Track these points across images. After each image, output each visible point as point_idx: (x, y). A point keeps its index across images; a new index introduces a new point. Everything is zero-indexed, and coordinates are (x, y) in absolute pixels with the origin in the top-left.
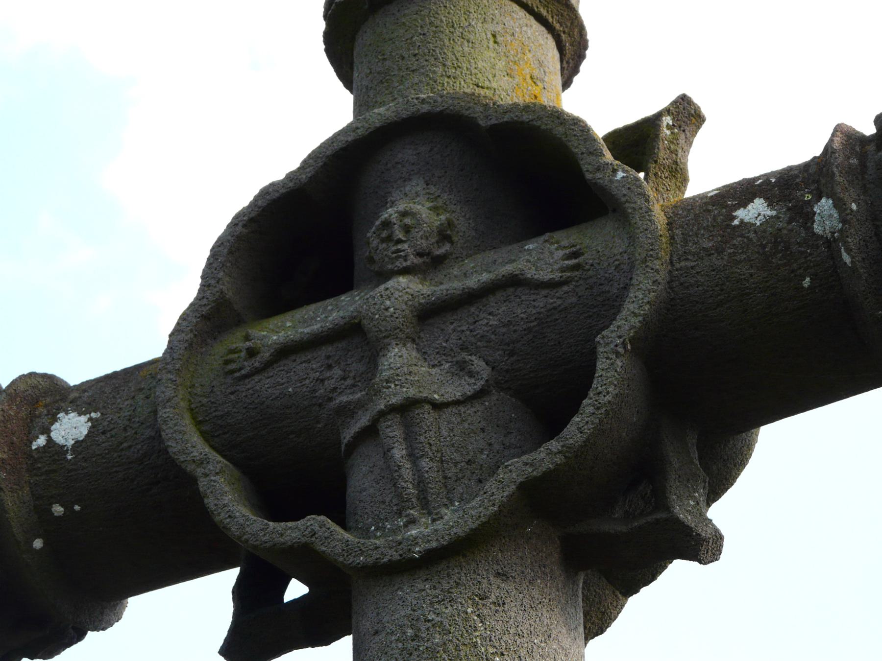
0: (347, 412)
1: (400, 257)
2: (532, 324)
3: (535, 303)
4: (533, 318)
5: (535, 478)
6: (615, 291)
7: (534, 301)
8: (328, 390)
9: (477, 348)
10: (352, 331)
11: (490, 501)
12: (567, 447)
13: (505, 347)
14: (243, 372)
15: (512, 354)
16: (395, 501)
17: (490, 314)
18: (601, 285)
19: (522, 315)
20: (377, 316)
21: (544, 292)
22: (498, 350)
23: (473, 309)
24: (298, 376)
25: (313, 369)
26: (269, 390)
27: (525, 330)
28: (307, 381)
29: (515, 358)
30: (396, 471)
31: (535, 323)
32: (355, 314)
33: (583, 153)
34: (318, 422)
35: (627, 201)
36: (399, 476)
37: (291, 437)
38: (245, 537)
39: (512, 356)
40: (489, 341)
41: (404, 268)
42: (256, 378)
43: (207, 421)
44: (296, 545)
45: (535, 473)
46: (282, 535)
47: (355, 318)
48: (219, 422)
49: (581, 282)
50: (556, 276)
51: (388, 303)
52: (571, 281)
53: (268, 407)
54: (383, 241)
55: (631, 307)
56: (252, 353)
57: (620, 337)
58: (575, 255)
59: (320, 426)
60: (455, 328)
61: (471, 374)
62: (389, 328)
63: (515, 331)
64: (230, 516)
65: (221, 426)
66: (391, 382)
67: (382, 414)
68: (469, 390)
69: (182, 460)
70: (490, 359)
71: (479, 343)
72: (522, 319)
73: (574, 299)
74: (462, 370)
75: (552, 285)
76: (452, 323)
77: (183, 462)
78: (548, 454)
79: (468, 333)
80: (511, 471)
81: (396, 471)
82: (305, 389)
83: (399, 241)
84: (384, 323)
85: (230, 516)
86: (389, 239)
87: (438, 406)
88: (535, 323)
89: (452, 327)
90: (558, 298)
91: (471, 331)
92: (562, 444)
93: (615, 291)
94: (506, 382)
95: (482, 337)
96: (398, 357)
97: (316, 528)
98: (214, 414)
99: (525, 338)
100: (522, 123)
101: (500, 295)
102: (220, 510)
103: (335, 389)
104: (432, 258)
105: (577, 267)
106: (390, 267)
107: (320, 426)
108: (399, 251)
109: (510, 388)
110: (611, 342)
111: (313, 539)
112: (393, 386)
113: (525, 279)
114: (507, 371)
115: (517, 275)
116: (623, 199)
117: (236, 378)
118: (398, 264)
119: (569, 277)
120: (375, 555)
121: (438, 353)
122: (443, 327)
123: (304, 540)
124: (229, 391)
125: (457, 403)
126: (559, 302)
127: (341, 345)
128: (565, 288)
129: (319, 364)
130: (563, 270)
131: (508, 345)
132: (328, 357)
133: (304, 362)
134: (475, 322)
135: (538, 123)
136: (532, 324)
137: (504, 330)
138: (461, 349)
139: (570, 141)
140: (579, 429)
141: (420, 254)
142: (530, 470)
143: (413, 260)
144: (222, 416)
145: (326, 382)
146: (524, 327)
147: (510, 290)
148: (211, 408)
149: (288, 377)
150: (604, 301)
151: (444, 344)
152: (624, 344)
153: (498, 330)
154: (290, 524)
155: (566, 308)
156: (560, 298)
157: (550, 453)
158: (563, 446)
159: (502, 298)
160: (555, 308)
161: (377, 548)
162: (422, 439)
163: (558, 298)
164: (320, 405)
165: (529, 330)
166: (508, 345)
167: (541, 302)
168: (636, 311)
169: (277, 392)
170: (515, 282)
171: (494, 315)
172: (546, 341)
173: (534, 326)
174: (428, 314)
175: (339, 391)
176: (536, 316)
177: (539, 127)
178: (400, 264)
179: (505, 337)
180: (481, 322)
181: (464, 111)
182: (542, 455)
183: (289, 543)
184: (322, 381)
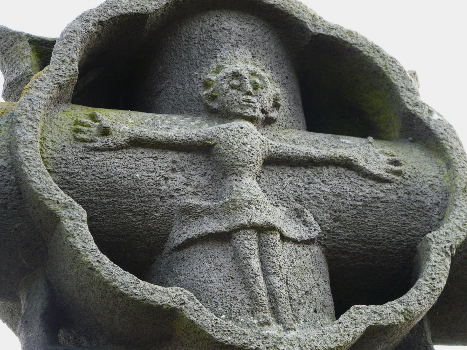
0: (190, 213)
1: (250, 106)
2: (358, 203)
3: (362, 188)
4: (359, 199)
5: (382, 326)
6: (429, 204)
7: (361, 185)
8: (171, 188)
9: (309, 204)
10: (203, 150)
11: (345, 331)
12: (408, 311)
13: (333, 213)
14: (96, 145)
15: (335, 220)
16: (247, 301)
17: (323, 181)
18: (417, 194)
19: (351, 193)
20: (236, 147)
21: (371, 182)
22: (326, 212)
23: (309, 172)
24: (145, 169)
25: (160, 167)
26: (118, 169)
27: (351, 205)
28: (153, 174)
29: (337, 224)
30: (253, 278)
31: (361, 203)
32: (210, 137)
33: (402, 87)
34: (156, 211)
35: (444, 139)
36: (255, 282)
37: (127, 214)
38: (114, 283)
39: (335, 221)
40: (320, 203)
41: (253, 116)
42: (107, 154)
43: (55, 172)
44: (165, 307)
45: (382, 322)
46: (152, 294)
47: (210, 140)
48: (67, 178)
49: (401, 186)
50: (385, 175)
51: (245, 140)
52: (393, 182)
53: (115, 182)
54: (233, 87)
55: (457, 222)
56: (105, 132)
57: (448, 242)
58: (396, 163)
59: (157, 215)
60: (292, 180)
61: (305, 223)
62: (246, 161)
63: (343, 203)
64: (98, 261)
65: (68, 182)
66: (252, 204)
67: (243, 227)
68: (306, 236)
69: (47, 197)
70: (319, 216)
71: (311, 201)
72: (350, 196)
73: (394, 197)
74: (299, 217)
75: (378, 179)
76: (289, 176)
77: (46, 199)
78: (393, 311)
79: (303, 189)
80: (361, 314)
81: (253, 278)
82: (151, 180)
83: (249, 94)
84: (241, 154)
85: (98, 261)
86: (239, 88)
87: (284, 238)
88: (361, 203)
89: (289, 179)
90: (381, 191)
91: (306, 189)
92: (404, 307)
93: (429, 204)
94: (325, 239)
95: (315, 197)
96: (248, 185)
97: (186, 299)
98: (63, 169)
99: (350, 212)
100: (346, 42)
101: (332, 169)
102: (88, 253)
103: (177, 190)
104: (266, 118)
105: (398, 173)
106: (239, 110)
107: (157, 215)
108: (249, 101)
109: (324, 246)
110: (441, 243)
111: (183, 307)
112: (254, 208)
113: (357, 166)
114: (328, 232)
115: (351, 160)
116: (441, 136)
117: (88, 147)
118: (248, 110)
119: (393, 178)
120: (243, 340)
121: (275, 195)
122: (281, 176)
123: (173, 305)
124: (79, 155)
125: (295, 241)
126: (382, 195)
127: (187, 156)
128: (388, 186)
129: (165, 165)
130: (388, 171)
131: (336, 212)
132: (174, 162)
133: (152, 157)
134: (309, 183)
135: (361, 49)
136: (358, 203)
137: (334, 199)
138: (296, 200)
139: (390, 73)
140: (418, 300)
141: (263, 111)
142: (379, 318)
143: (258, 114)
144: (71, 174)
145: (170, 181)
146: (351, 203)
147: (342, 170)
148: (61, 163)
149: (136, 165)
150: (419, 208)
151: (281, 191)
152: (451, 248)
153: (328, 197)
154: (159, 288)
155: (387, 202)
156: (384, 192)
157: (395, 311)
158: (405, 309)
159: (334, 173)
160: (378, 198)
161: (244, 334)
162: (275, 259)
163: (381, 191)
164: (162, 198)
165: (355, 207)
166: (336, 212)
167: (367, 189)
168: (461, 226)
169: (126, 174)
170: (347, 165)
171: (328, 183)
172: (367, 220)
173: (359, 205)
174: (275, 161)
175: (181, 193)
176: (363, 198)
177: (361, 52)
178: (249, 112)
179: (335, 204)
180: (315, 185)
181: (294, 13)
182: (389, 311)
183: (159, 303)
184: (166, 179)
